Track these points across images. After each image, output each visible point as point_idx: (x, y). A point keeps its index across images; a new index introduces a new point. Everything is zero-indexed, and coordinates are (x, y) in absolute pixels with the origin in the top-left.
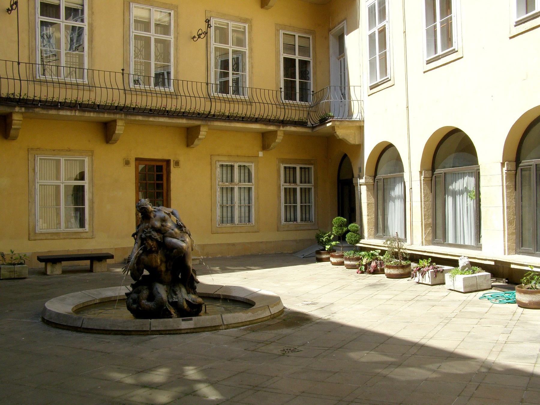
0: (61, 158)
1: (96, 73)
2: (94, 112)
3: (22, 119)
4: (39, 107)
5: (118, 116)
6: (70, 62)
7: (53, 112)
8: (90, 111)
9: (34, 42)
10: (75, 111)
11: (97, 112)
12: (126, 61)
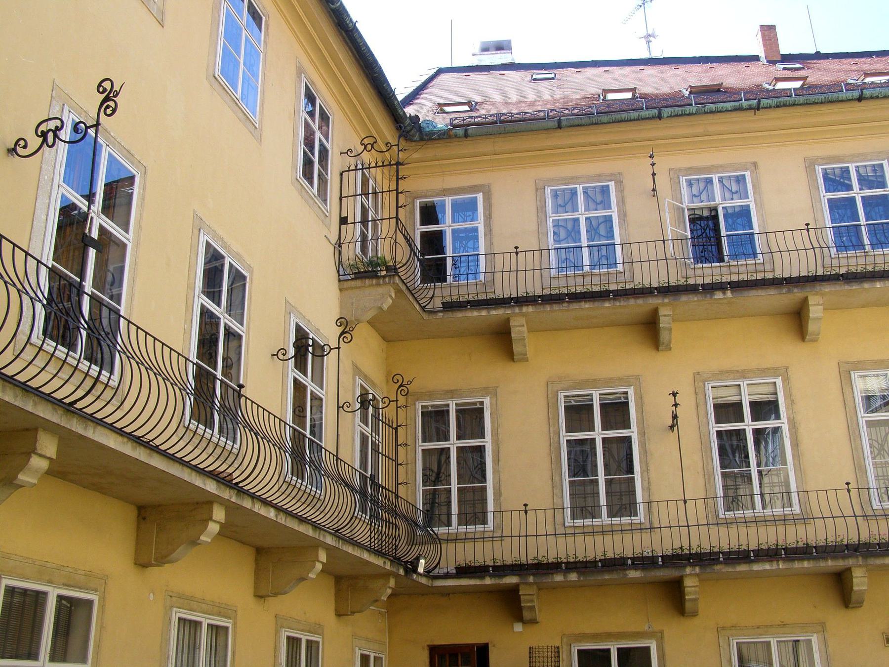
0: (771, 640)
1: (813, 496)
2: (808, 559)
3: (697, 584)
4: (721, 563)
5: (850, 562)
6: (884, 476)
7: (742, 568)
8: (802, 559)
9: (710, 463)
10: (778, 561)
11: (814, 558)
12: (859, 468)
